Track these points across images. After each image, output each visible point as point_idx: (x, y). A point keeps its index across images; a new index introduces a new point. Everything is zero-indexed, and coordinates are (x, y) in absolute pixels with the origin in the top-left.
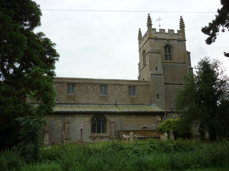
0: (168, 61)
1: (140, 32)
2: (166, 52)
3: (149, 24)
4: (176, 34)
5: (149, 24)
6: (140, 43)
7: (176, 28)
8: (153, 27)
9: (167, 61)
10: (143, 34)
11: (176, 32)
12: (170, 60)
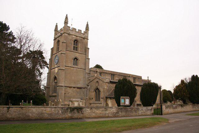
0: (97, 102)
1: (57, 26)
2: (74, 44)
3: (66, 22)
4: (82, 34)
5: (66, 22)
6: (56, 34)
7: (83, 30)
8: (69, 25)
9: (74, 51)
10: (59, 29)
11: (83, 32)
12: (76, 50)
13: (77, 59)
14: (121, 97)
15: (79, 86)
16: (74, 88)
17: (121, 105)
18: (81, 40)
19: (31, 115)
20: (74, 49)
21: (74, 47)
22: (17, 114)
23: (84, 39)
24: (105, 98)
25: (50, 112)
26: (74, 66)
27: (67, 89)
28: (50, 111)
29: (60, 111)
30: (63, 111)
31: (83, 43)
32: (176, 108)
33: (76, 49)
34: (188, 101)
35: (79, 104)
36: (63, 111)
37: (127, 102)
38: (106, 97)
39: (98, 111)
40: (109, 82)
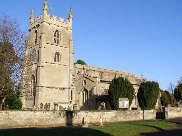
2: (55, 36)
9: (55, 44)
13: (59, 54)
14: (119, 99)
15: (62, 86)
16: (56, 88)
17: (120, 108)
18: (64, 31)
19: (18, 121)
20: (55, 42)
21: (55, 39)
22: (3, 120)
23: (67, 29)
24: (95, 100)
25: (41, 117)
26: (55, 62)
27: (48, 90)
28: (40, 116)
29: (52, 116)
30: (55, 116)
31: (65, 34)
32: (181, 112)
33: (57, 41)
34: (171, 96)
35: (69, 107)
36: (55, 116)
37: (126, 102)
38: (96, 100)
39: (94, 116)
40: (100, 81)
